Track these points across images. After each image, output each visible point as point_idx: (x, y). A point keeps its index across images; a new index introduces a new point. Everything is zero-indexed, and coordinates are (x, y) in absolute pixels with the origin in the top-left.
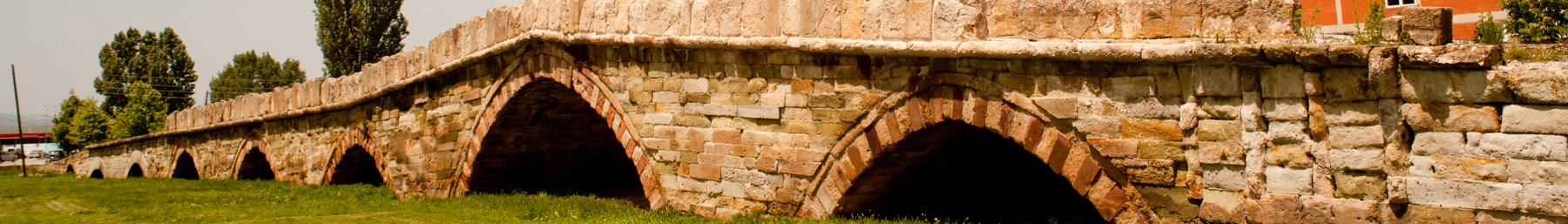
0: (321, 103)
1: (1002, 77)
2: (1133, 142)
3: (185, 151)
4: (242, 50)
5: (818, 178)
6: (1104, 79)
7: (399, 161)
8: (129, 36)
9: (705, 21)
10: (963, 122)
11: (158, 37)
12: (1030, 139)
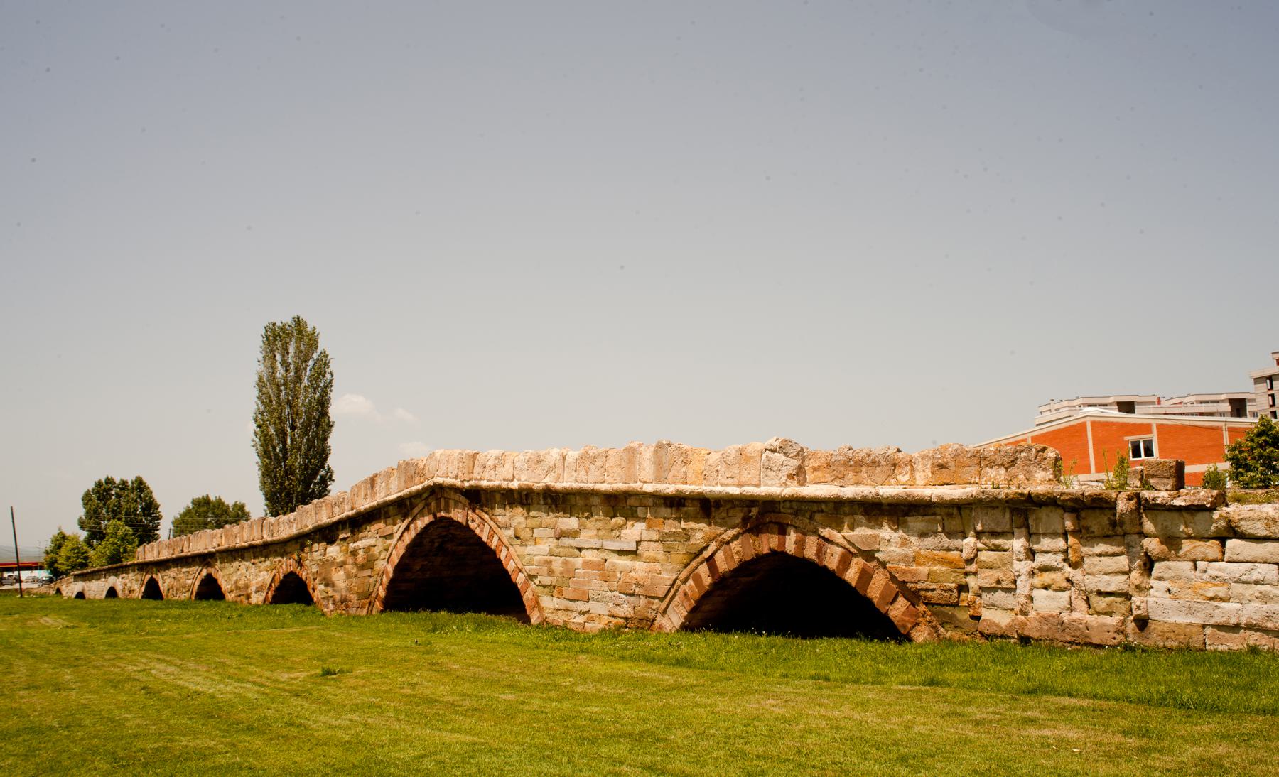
0: (263, 538)
1: (818, 517)
2: (924, 570)
3: (152, 577)
4: (199, 495)
5: (668, 599)
6: (900, 518)
7: (327, 585)
8: (107, 483)
9: (576, 471)
10: (786, 553)
11: (130, 484)
12: (841, 567)
